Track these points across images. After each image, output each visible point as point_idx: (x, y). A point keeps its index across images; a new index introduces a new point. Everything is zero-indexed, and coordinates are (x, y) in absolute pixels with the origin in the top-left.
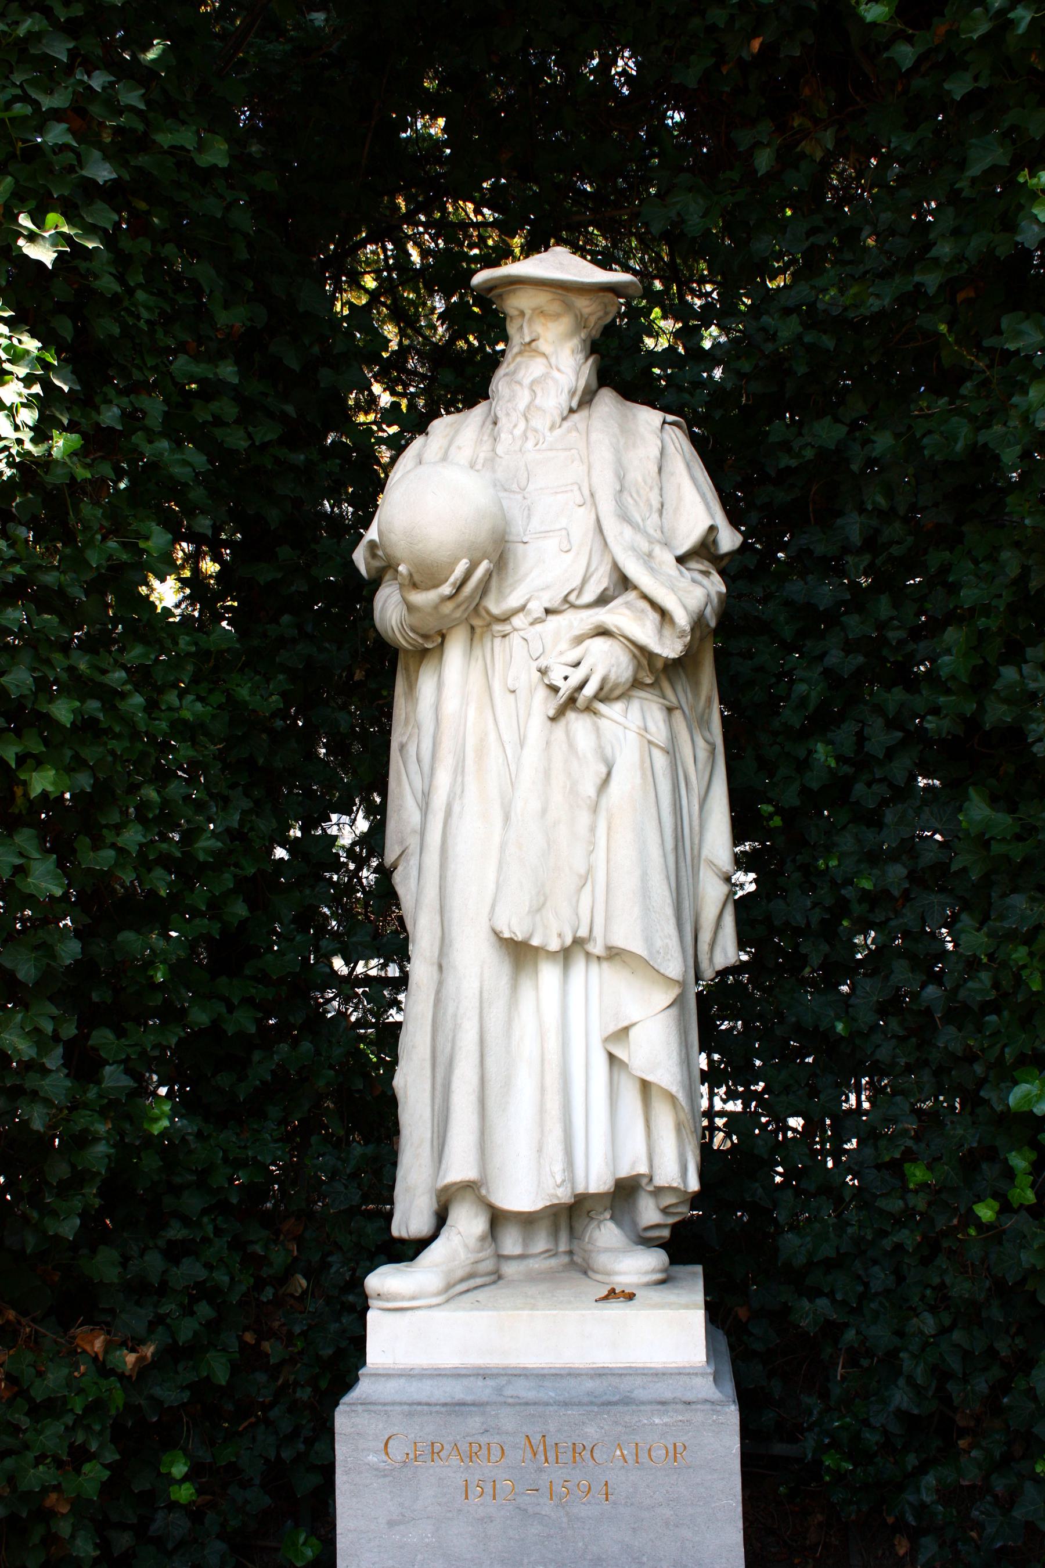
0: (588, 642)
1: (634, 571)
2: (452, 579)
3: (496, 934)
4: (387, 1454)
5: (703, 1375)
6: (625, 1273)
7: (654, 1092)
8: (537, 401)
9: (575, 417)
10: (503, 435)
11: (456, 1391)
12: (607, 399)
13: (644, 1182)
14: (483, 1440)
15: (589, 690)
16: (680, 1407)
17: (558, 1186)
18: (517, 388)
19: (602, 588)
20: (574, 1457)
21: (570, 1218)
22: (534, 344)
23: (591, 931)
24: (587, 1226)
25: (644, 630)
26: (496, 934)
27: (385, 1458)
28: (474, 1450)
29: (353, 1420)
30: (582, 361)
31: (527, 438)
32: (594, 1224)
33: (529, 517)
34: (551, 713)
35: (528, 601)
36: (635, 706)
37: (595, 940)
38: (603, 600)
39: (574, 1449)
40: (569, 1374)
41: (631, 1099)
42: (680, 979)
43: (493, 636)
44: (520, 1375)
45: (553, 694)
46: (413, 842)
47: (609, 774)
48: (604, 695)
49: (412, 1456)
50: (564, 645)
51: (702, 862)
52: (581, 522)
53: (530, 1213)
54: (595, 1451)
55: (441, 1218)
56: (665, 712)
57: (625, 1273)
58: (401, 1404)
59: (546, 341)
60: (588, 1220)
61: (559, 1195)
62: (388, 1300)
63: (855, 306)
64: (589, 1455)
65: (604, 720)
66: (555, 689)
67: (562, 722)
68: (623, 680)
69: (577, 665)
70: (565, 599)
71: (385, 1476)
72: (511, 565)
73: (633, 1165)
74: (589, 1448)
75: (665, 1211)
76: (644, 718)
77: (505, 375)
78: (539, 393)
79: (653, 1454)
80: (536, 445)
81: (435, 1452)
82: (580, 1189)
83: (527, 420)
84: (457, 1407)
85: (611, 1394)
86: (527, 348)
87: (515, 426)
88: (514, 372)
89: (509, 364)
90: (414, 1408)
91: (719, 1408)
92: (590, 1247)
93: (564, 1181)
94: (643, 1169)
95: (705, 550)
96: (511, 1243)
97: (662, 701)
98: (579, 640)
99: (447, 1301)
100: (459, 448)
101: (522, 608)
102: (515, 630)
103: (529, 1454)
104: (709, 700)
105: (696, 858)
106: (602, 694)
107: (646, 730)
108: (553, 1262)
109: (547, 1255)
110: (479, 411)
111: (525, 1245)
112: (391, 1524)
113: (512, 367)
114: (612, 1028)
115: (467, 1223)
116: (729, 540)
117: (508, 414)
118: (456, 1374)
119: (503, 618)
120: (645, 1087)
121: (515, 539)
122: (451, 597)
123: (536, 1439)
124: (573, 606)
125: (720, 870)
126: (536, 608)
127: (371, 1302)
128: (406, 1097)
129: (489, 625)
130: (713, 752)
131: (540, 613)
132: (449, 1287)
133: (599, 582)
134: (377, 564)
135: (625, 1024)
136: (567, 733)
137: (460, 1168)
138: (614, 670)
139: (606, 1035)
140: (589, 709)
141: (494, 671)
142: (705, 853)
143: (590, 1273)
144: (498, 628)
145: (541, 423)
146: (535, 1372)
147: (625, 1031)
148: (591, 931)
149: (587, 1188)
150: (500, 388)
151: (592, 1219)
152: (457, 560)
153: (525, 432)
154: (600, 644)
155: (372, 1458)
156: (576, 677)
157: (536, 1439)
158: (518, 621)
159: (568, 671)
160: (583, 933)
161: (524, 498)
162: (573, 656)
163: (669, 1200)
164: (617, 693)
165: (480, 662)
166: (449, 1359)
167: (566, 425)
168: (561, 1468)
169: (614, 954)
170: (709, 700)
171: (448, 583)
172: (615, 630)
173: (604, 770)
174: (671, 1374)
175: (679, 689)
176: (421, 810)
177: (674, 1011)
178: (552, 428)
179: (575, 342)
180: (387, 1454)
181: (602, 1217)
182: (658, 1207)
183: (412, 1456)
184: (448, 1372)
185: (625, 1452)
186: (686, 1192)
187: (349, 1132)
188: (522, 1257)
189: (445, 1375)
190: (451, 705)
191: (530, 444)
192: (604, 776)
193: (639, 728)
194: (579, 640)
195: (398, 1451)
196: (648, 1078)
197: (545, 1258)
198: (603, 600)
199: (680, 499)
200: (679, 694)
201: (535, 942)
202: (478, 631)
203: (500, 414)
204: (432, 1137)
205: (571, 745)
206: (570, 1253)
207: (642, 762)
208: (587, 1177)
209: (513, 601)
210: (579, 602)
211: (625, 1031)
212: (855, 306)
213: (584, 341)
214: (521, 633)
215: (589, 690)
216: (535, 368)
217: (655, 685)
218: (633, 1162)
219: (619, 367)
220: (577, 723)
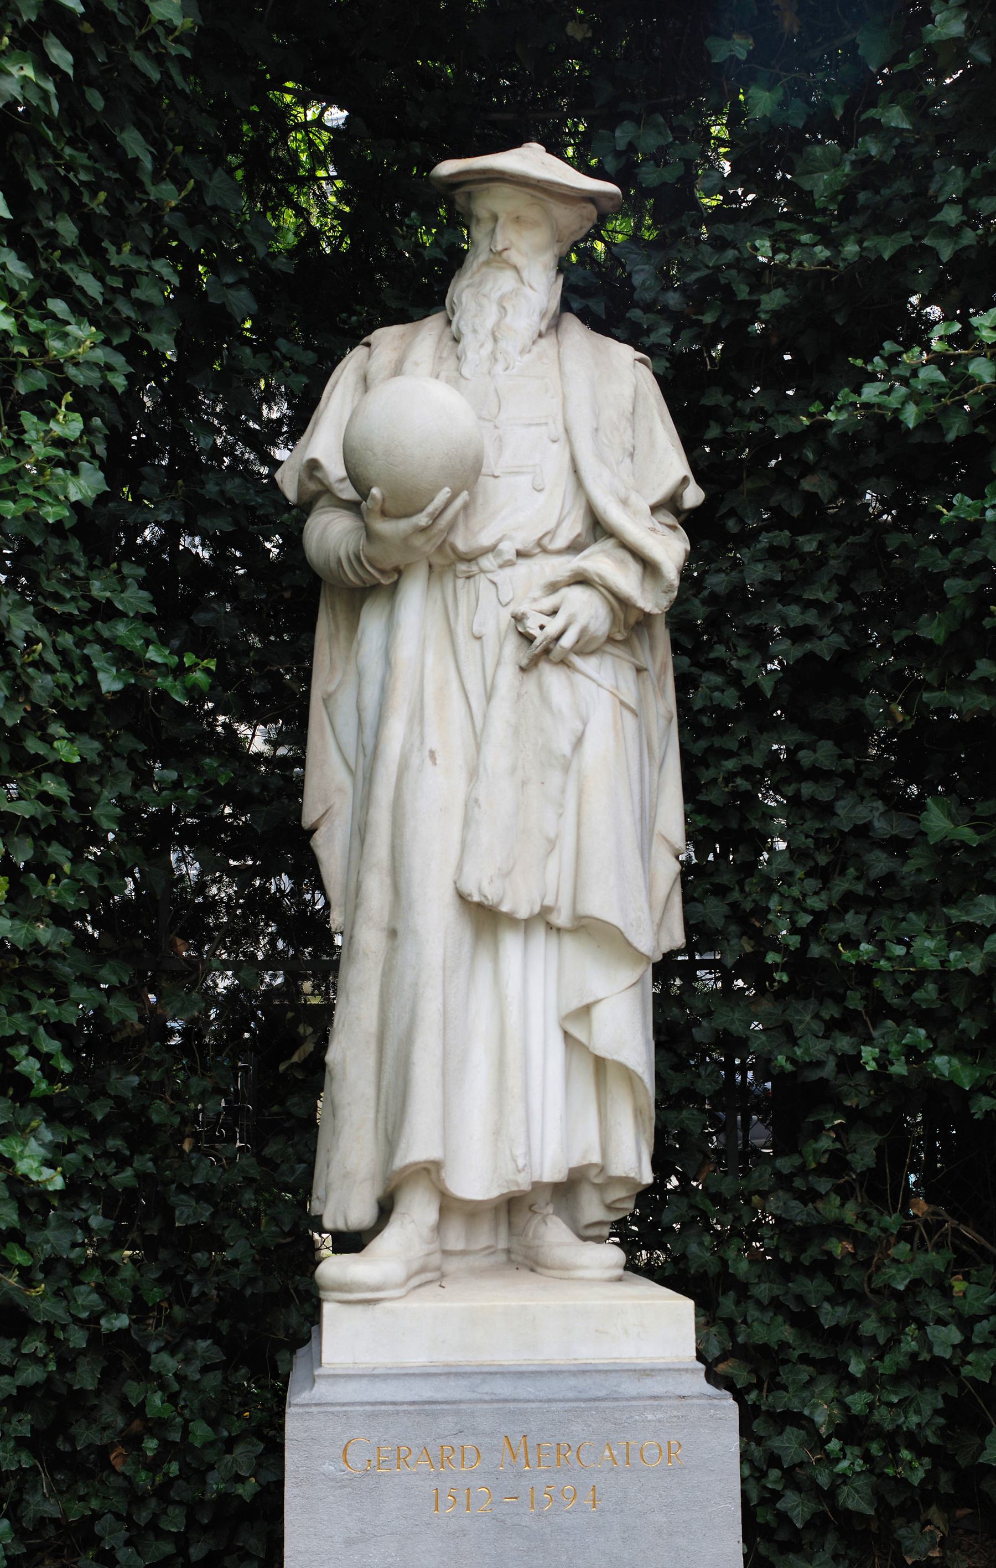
0: (565, 591)
1: (615, 515)
2: (430, 509)
3: (462, 897)
4: (346, 1461)
5: (693, 1371)
6: (587, 1267)
7: (612, 1075)
9: (543, 342)
10: (470, 355)
11: (425, 1391)
12: (574, 329)
14: (456, 1442)
15: (567, 641)
16: (675, 1402)
19: (575, 534)
20: (559, 1459)
21: (509, 1212)
23: (557, 900)
24: (529, 1221)
25: (627, 580)
26: (462, 897)
27: (344, 1466)
28: (446, 1453)
29: (307, 1423)
31: (496, 360)
32: (538, 1218)
33: (500, 449)
34: (524, 662)
35: (500, 540)
37: (559, 911)
38: (575, 548)
39: (558, 1450)
40: (551, 1372)
43: (456, 576)
44: (496, 1373)
45: (526, 643)
48: (585, 647)
49: (374, 1463)
50: (537, 593)
51: (655, 837)
52: (557, 459)
54: (582, 1451)
55: (386, 1209)
56: (634, 673)
57: (587, 1267)
58: (362, 1404)
59: (519, 251)
60: (530, 1214)
61: (520, 1181)
62: (350, 1291)
64: (575, 1457)
65: (578, 678)
66: (528, 639)
67: (533, 675)
68: (600, 633)
69: (554, 613)
70: (539, 543)
71: (344, 1487)
74: (574, 1449)
75: (610, 1208)
76: (616, 678)
78: (510, 311)
79: (645, 1454)
80: (506, 369)
81: (400, 1458)
83: (495, 340)
84: (427, 1409)
85: (596, 1392)
86: (497, 258)
87: (482, 346)
88: (480, 283)
89: (473, 274)
90: (377, 1411)
91: (716, 1402)
92: (537, 1242)
94: (595, 1158)
95: (670, 505)
97: (633, 660)
98: (553, 588)
99: (408, 1292)
100: (416, 364)
101: (492, 549)
102: (482, 571)
103: (508, 1457)
104: (664, 666)
105: (652, 830)
107: (617, 688)
108: (492, 1260)
110: (431, 326)
111: (468, 1241)
112: (349, 1542)
113: (477, 278)
114: (575, 1004)
115: (417, 1215)
116: (694, 496)
117: (475, 331)
118: (425, 1375)
119: (470, 557)
123: (516, 1440)
124: (545, 551)
126: (509, 549)
127: (323, 1295)
128: (344, 1074)
129: (452, 565)
131: (511, 555)
132: (409, 1278)
134: (312, 487)
135: (591, 1000)
136: (540, 686)
138: (593, 621)
139: (565, 1012)
140: (564, 662)
141: (457, 615)
142: (659, 827)
143: (539, 1269)
144: (462, 567)
145: (510, 345)
146: (513, 1369)
147: (586, 1010)
148: (557, 900)
149: (346, 1223)
150: (464, 300)
151: (535, 1212)
152: (438, 489)
153: (493, 353)
154: (578, 595)
155: (328, 1468)
156: (554, 626)
157: (516, 1440)
158: (487, 562)
159: (544, 620)
160: (549, 901)
161: (496, 427)
162: (548, 603)
163: (618, 1193)
164: (593, 647)
165: (439, 602)
166: (416, 1356)
167: (535, 349)
168: (543, 1472)
171: (424, 513)
172: (597, 579)
174: (660, 1370)
177: (637, 989)
178: (522, 352)
180: (346, 1461)
181: (545, 1212)
182: (603, 1202)
183: (374, 1463)
184: (416, 1371)
185: (615, 1453)
186: (640, 1184)
188: (463, 1253)
189: (413, 1375)
190: (406, 649)
191: (499, 368)
194: (553, 588)
195: (358, 1459)
198: (575, 548)
199: (652, 445)
201: (505, 908)
202: (436, 569)
203: (464, 330)
204: (377, 1118)
205: (545, 699)
206: (508, 1251)
207: (615, 723)
208: (542, 1164)
209: (485, 540)
210: (552, 547)
211: (586, 1010)
214: (490, 576)
215: (567, 641)
216: (505, 281)
217: (626, 642)
218: (587, 1150)
219: (595, 297)
220: (552, 676)
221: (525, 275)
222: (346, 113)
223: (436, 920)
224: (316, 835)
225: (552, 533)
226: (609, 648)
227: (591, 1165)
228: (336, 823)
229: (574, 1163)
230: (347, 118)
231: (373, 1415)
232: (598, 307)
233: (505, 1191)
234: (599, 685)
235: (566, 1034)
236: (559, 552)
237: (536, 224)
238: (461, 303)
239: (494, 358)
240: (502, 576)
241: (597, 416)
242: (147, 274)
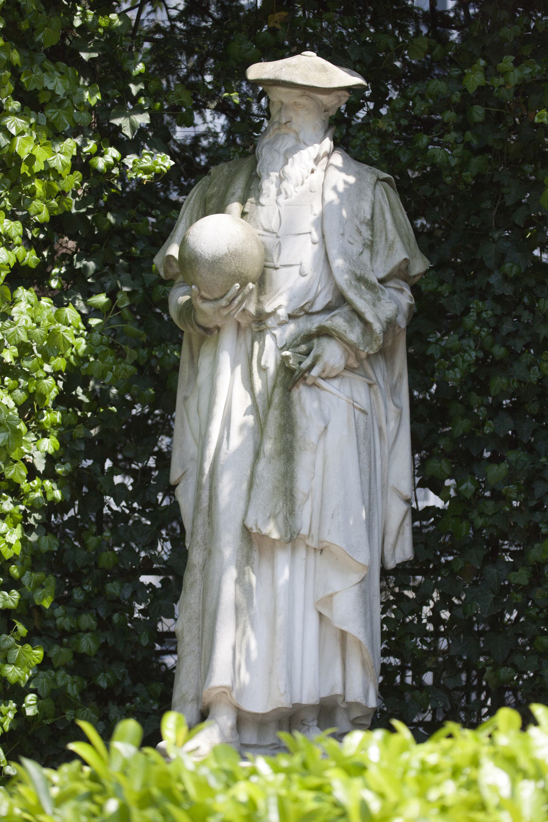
13: (340, 700)
17: (282, 695)
18: (275, 155)
19: (327, 301)
22: (288, 124)
30: (322, 135)
41: (333, 648)
42: (367, 564)
46: (192, 468)
47: (326, 428)
53: (263, 715)
56: (367, 387)
63: (324, 371)
72: (267, 284)
73: (333, 688)
76: (352, 391)
77: (267, 143)
82: (296, 700)
93: (285, 692)
94: (339, 691)
95: (401, 273)
101: (274, 313)
104: (400, 376)
106: (324, 375)
109: (272, 747)
120: (343, 635)
122: (226, 307)
125: (401, 494)
130: (400, 415)
133: (326, 296)
135: (330, 592)
149: (301, 700)
150: (263, 153)
164: (334, 374)
170: (400, 376)
173: (322, 425)
176: (198, 446)
181: (311, 724)
186: (366, 707)
187: (462, 70)
192: (322, 429)
193: (348, 397)
196: (344, 628)
197: (272, 750)
198: (328, 309)
200: (379, 373)
212: (324, 371)
213: (324, 121)
218: (333, 685)
221: (301, 136)
222: (173, 163)
223: (228, 546)
224: (178, 487)
225: (312, 303)
226: (347, 374)
227: (337, 695)
228: (190, 481)
229: (324, 694)
230: (172, 167)
233: (275, 707)
234: (339, 397)
235: (320, 615)
236: (318, 313)
237: (79, 639)
238: (262, 153)
239: (279, 193)
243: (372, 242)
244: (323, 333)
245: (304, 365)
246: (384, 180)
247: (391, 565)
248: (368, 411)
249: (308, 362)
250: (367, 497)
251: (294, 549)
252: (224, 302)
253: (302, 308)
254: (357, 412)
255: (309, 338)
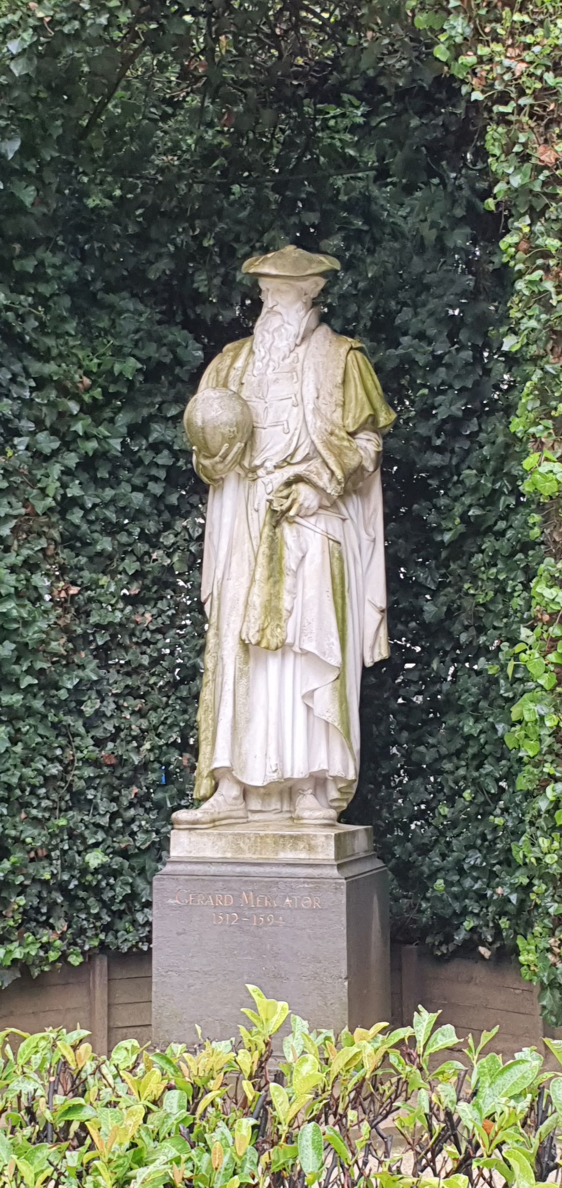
8: (275, 344)
11: (213, 869)
36: (322, 518)
41: (319, 730)
47: (304, 557)
69: (287, 497)
82: (288, 775)
94: (325, 767)
95: (371, 423)
96: (255, 804)
101: (262, 465)
112: (179, 934)
115: (228, 791)
120: (327, 723)
121: (260, 425)
124: (289, 464)
126: (269, 465)
131: (271, 468)
137: (222, 760)
142: (368, 597)
160: (289, 640)
164: (310, 513)
169: (305, 653)
173: (300, 555)
175: (351, 507)
179: (299, 305)
198: (306, 459)
210: (294, 461)
216: (276, 322)
218: (320, 764)
226: (321, 511)
231: (187, 880)
232: (338, 323)
240: (267, 479)
241: (318, 390)
242: (517, 197)
243: (344, 402)
244: (298, 479)
245: (284, 508)
246: (357, 349)
247: (369, 663)
248: (341, 540)
249: (287, 503)
250: (340, 615)
251: (283, 654)
252: (217, 459)
253: (285, 460)
254: (331, 542)
255: (288, 484)
